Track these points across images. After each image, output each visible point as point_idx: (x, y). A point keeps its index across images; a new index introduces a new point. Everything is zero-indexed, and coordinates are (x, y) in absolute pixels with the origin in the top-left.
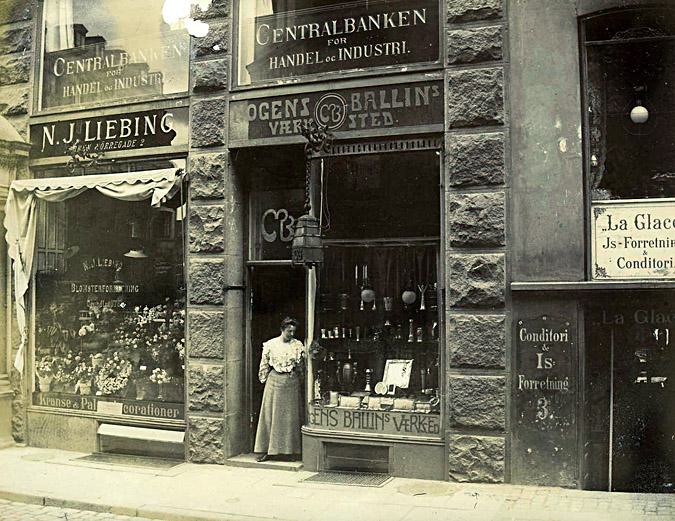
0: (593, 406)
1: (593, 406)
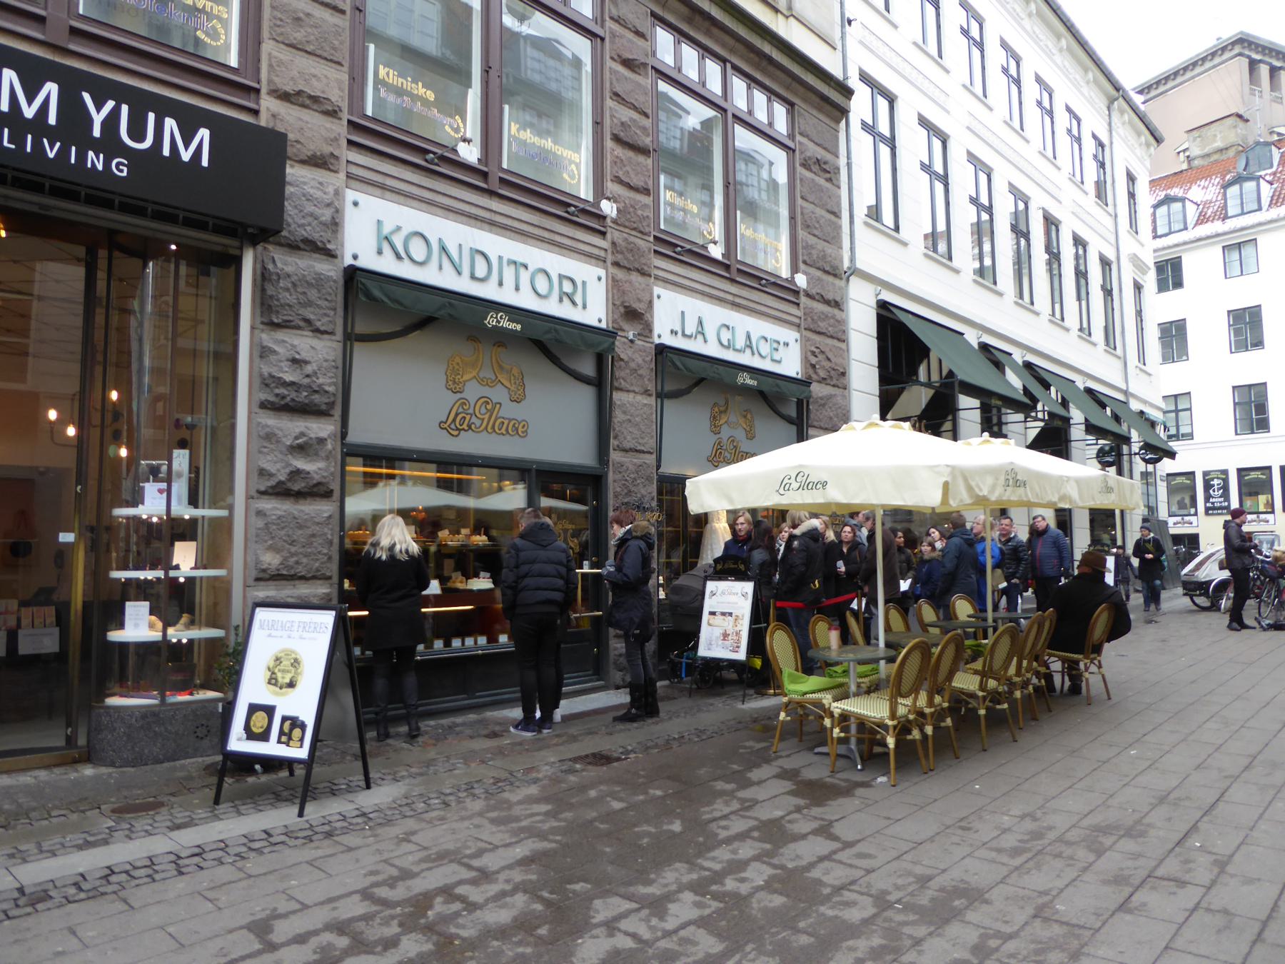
0: (396, 922)
1: (396, 922)
